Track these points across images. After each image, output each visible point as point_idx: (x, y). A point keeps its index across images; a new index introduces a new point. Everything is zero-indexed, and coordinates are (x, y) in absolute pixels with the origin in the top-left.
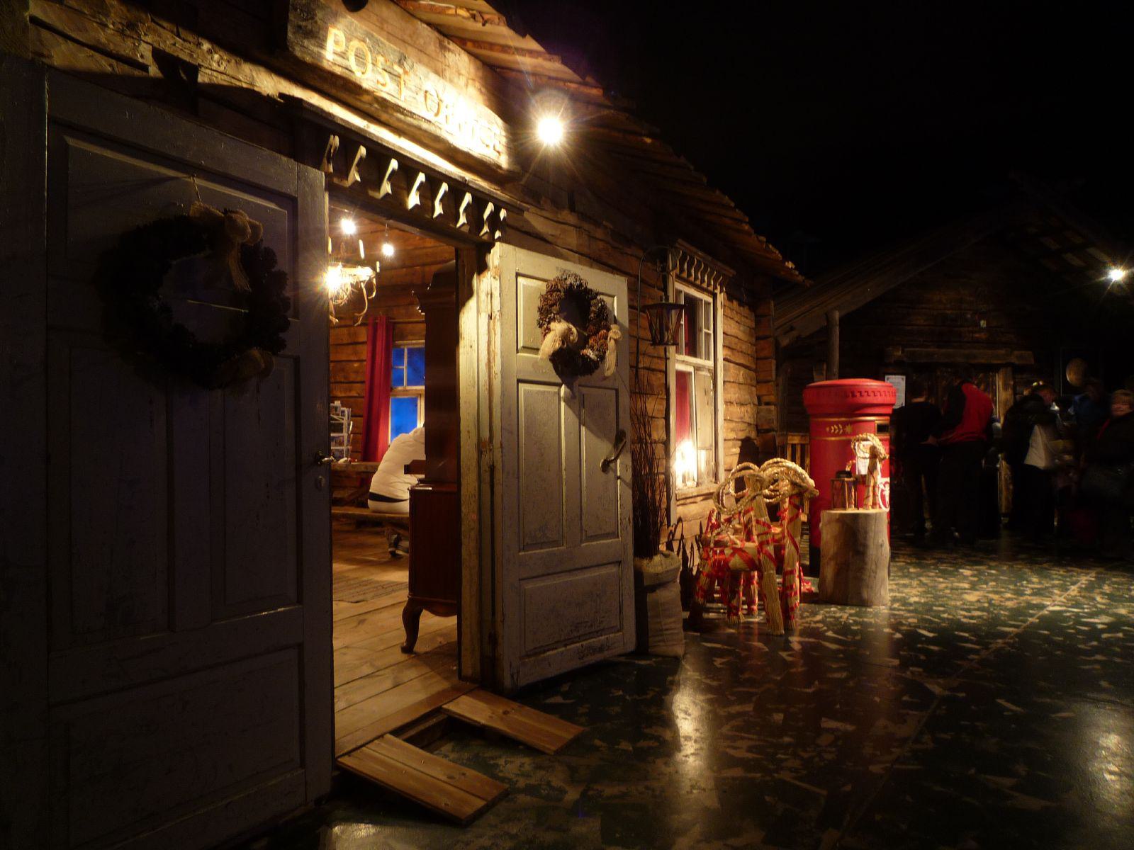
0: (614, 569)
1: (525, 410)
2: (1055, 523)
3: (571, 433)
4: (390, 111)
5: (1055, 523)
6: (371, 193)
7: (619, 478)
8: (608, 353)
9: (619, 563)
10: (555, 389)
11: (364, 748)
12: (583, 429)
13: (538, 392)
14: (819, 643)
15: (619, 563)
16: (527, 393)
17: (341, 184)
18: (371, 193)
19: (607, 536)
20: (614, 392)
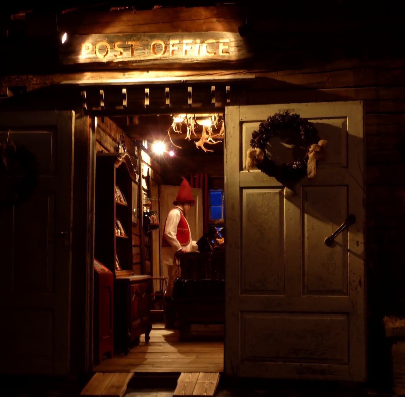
0: (342, 318)
1: (247, 206)
2: (172, 299)
3: (291, 219)
4: (129, 64)
5: (172, 299)
6: (118, 108)
7: (348, 251)
8: (309, 161)
9: (347, 314)
10: (278, 190)
11: (198, 382)
12: (306, 216)
13: (259, 194)
14: (136, 373)
15: (347, 314)
16: (249, 195)
17: (98, 109)
18: (118, 108)
19: (340, 292)
20: (346, 187)
